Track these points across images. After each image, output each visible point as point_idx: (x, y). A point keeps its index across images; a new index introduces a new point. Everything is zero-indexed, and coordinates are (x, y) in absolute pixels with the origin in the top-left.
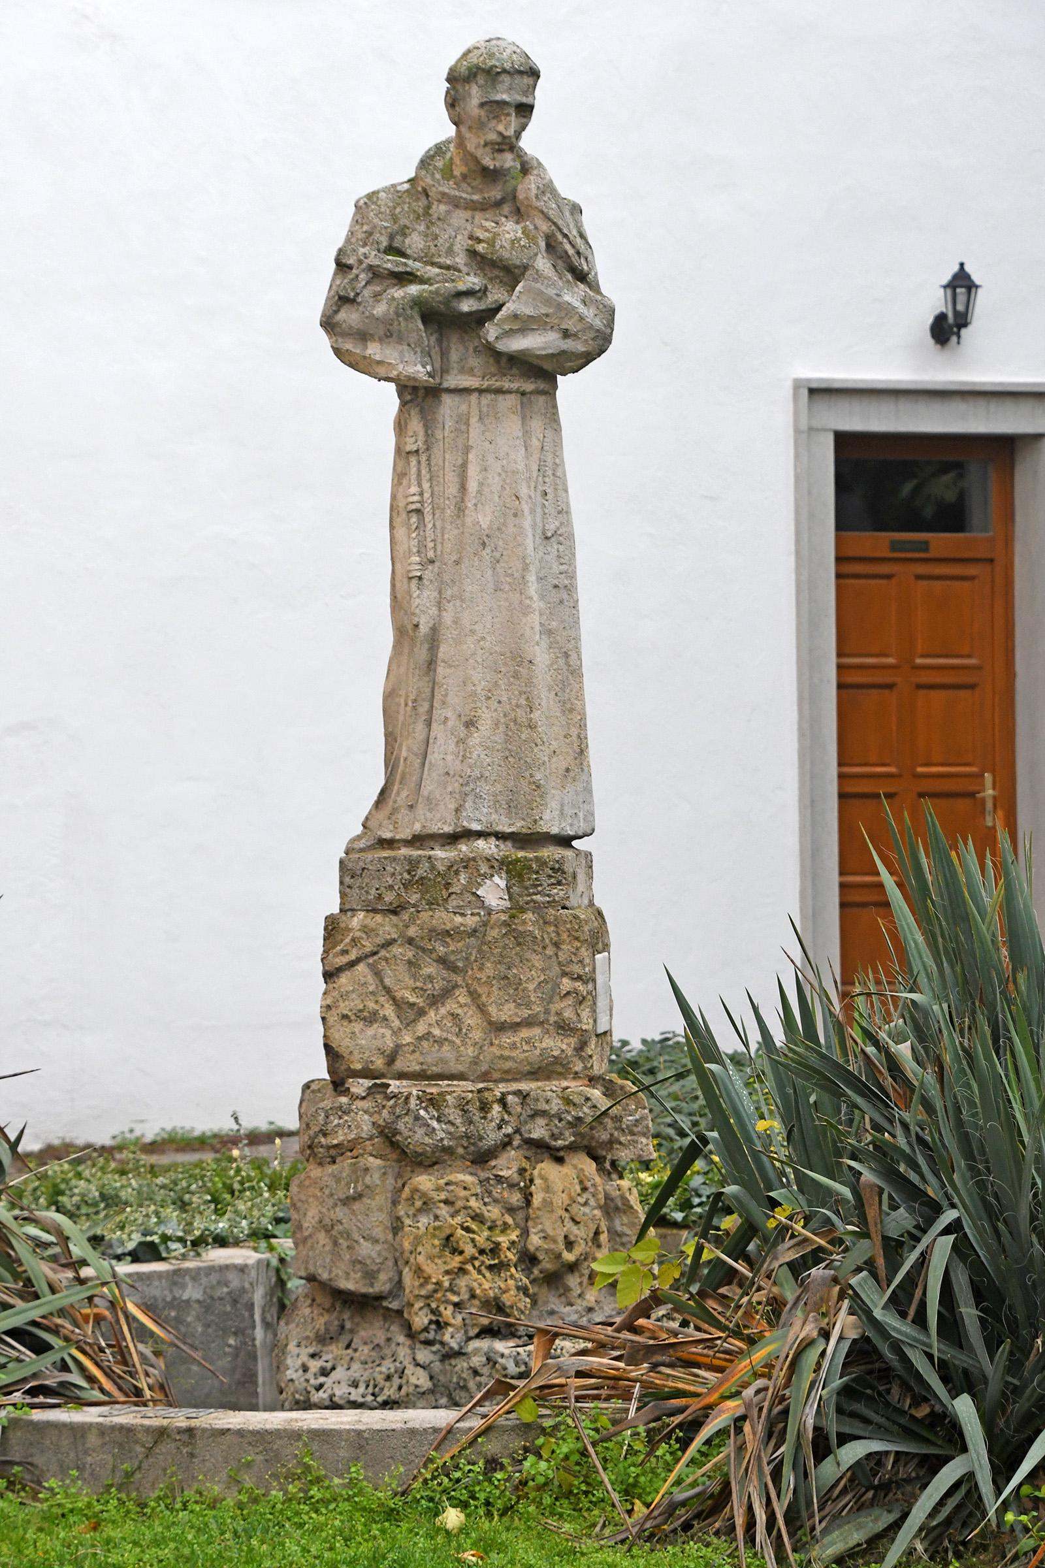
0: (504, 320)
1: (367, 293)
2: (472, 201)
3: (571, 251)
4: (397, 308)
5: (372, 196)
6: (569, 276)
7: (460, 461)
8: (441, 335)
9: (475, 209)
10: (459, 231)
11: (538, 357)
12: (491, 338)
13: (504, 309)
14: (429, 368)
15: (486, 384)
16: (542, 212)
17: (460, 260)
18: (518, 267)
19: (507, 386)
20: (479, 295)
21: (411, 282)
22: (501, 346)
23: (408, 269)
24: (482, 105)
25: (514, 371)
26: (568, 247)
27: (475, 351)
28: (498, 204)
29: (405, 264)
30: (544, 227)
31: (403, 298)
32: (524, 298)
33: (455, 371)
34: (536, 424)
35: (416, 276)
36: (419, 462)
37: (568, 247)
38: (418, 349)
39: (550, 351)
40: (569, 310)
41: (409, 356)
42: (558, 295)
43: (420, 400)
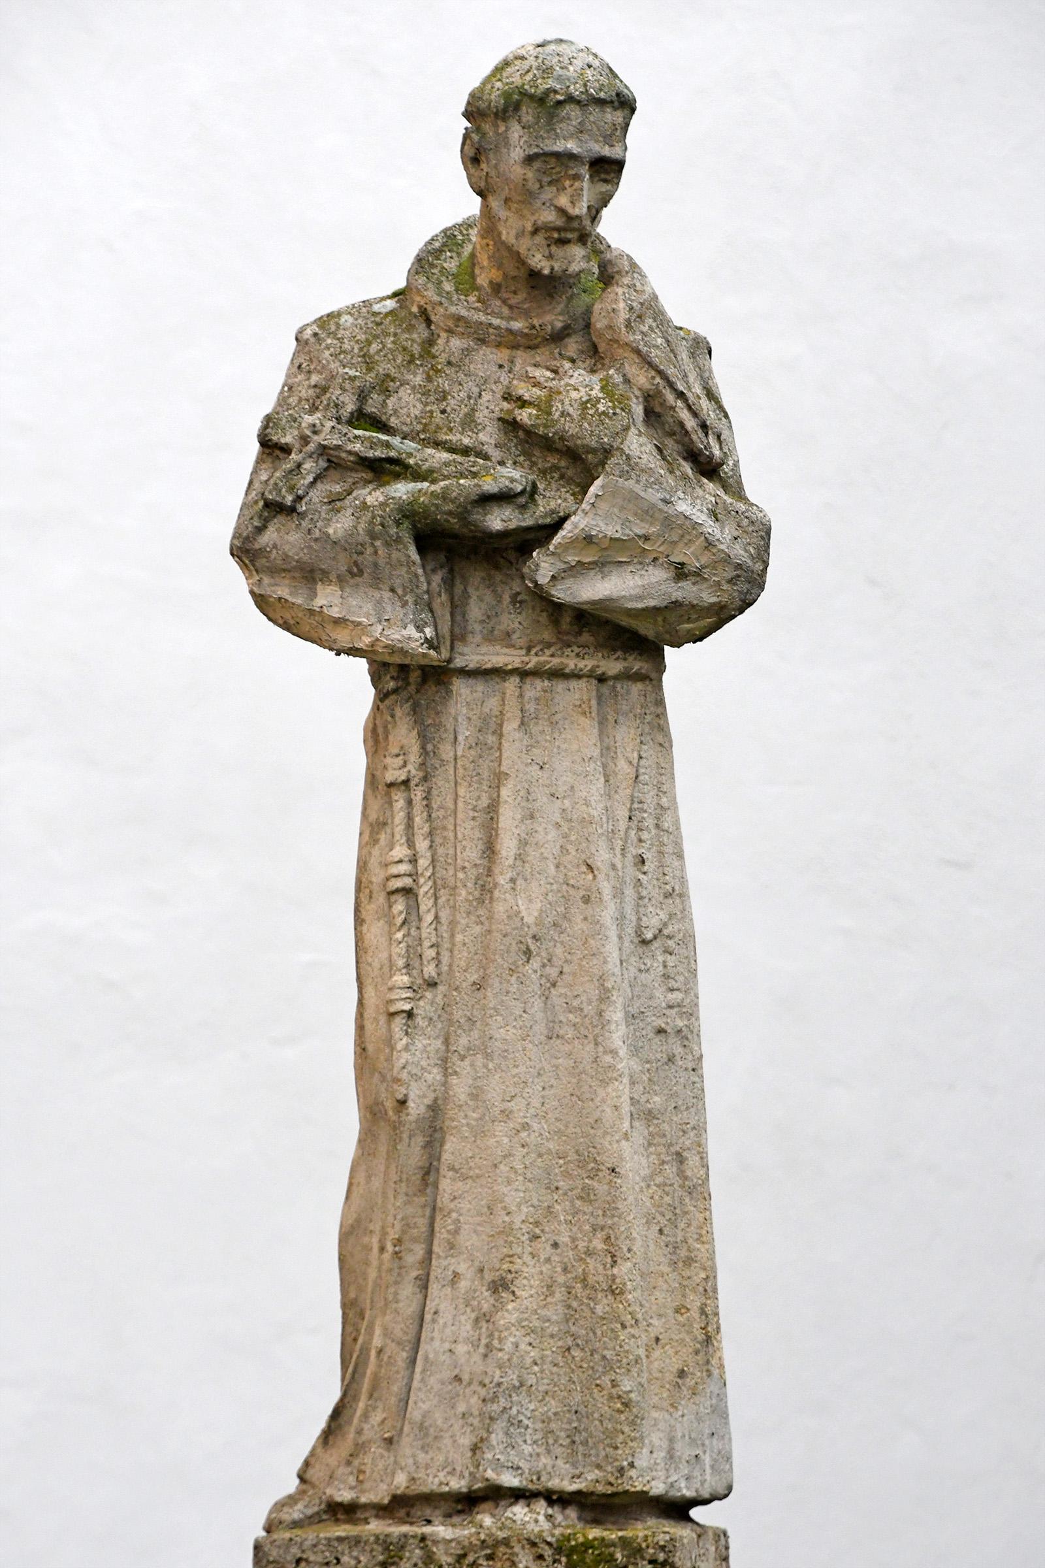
1: (316, 495)
2: (510, 331)
3: (690, 423)
4: (371, 523)
6: (687, 468)
7: (485, 801)
9: (515, 347)
10: (487, 383)
11: (630, 612)
12: (543, 578)
13: (568, 525)
14: (429, 632)
15: (533, 662)
16: (638, 352)
17: (488, 437)
18: (594, 451)
19: (571, 664)
20: (522, 500)
21: (397, 477)
22: (560, 593)
23: (393, 454)
24: (529, 160)
25: (586, 637)
26: (685, 415)
28: (558, 337)
29: (387, 445)
31: (383, 505)
32: (603, 506)
33: (478, 638)
34: (625, 735)
35: (407, 467)
36: (410, 802)
37: (685, 415)
38: (410, 599)
40: (689, 528)
41: (393, 610)
43: (412, 688)
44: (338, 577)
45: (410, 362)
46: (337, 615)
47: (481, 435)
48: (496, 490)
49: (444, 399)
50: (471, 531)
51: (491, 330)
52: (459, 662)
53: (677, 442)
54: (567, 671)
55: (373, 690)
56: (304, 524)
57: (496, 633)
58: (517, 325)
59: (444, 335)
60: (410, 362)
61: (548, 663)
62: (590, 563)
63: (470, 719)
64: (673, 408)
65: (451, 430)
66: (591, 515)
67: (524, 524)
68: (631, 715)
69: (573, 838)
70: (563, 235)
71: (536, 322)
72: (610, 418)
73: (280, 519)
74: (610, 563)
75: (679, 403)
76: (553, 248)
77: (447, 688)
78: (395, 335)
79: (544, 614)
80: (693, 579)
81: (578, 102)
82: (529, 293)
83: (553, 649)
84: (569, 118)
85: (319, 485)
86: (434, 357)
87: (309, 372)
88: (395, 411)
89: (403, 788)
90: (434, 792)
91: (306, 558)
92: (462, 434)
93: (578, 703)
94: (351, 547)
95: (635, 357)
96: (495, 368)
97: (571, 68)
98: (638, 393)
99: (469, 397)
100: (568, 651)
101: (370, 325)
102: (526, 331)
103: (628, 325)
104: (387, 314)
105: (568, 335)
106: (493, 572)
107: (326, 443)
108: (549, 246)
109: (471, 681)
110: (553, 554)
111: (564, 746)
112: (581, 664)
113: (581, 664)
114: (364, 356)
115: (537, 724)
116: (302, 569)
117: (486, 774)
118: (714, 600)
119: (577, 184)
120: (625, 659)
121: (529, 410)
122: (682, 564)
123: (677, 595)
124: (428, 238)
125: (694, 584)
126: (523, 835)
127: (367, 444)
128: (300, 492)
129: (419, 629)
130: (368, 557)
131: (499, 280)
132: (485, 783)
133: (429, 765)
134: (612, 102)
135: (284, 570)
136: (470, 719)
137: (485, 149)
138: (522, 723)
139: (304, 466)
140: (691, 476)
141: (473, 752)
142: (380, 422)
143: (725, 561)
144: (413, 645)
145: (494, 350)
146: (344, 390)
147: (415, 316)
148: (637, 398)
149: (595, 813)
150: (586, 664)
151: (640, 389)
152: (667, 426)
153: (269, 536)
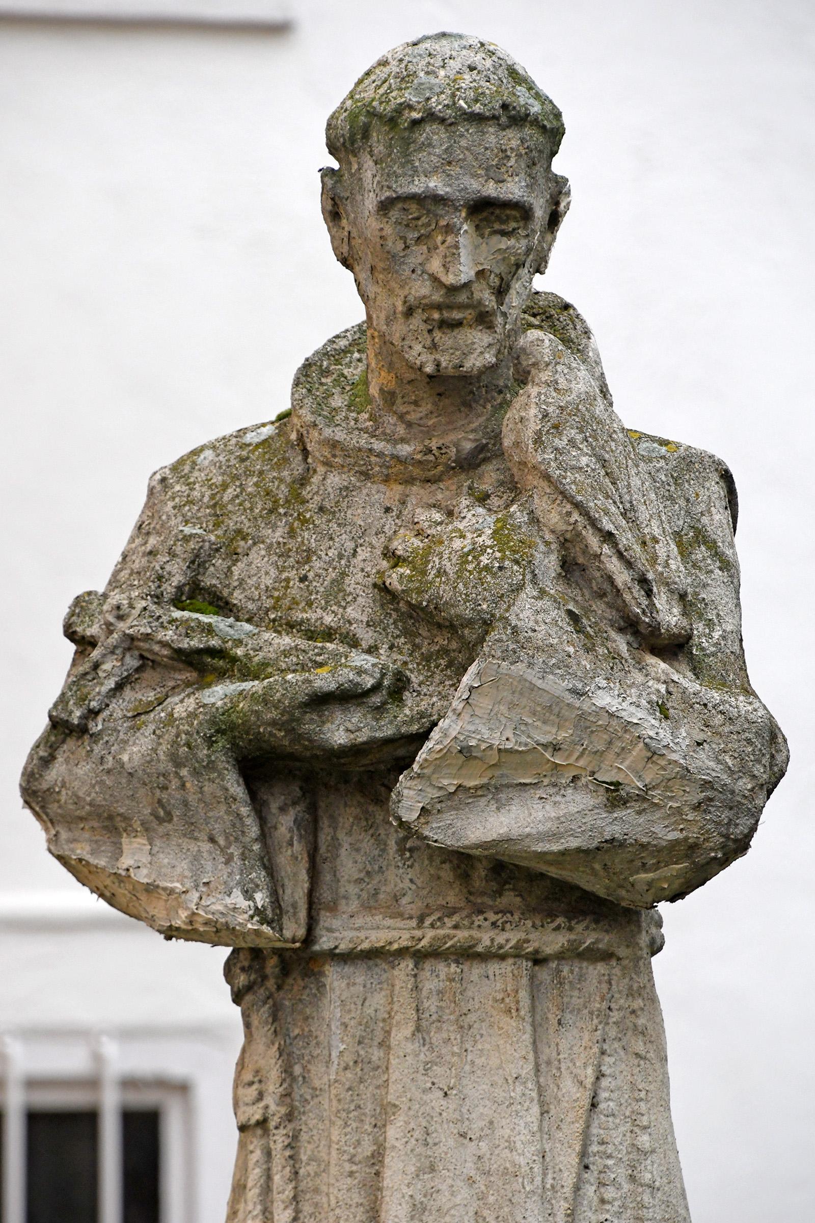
0: (442, 760)
1: (119, 708)
2: (396, 458)
3: (622, 577)
4: (174, 743)
5: (183, 467)
6: (621, 643)
7: (367, 1148)
8: (313, 809)
9: (409, 481)
10: (369, 533)
11: (541, 856)
12: (410, 815)
13: (435, 735)
14: (261, 898)
15: (427, 938)
16: (547, 477)
17: (359, 611)
18: (470, 623)
19: (486, 939)
20: (376, 699)
21: (222, 675)
22: (439, 832)
23: (214, 642)
24: (385, 207)
25: (509, 898)
26: (614, 565)
27: (401, 850)
28: (469, 464)
29: (209, 630)
30: (554, 516)
31: (192, 715)
32: (483, 703)
33: (354, 905)
34: (575, 1045)
35: (234, 660)
36: (268, 1154)
37: (614, 565)
38: (235, 850)
39: (574, 843)
40: (619, 731)
41: (214, 870)
42: (574, 692)
43: (271, 984)
44: (143, 824)
45: (271, 511)
46: (145, 881)
47: (349, 610)
48: (333, 686)
49: (308, 560)
50: (306, 748)
51: (373, 459)
52: (324, 943)
53: (610, 606)
54: (480, 949)
55: (228, 987)
56: (97, 748)
57: (381, 896)
58: (405, 450)
59: (321, 469)
60: (271, 511)
61: (450, 937)
62: (476, 788)
63: (346, 1026)
64: (597, 556)
65: (310, 604)
66: (466, 716)
67: (379, 735)
68: (586, 1011)
69: (491, 1199)
70: (446, 314)
71: (434, 445)
72: (494, 575)
73: (71, 744)
74: (508, 786)
75: (606, 549)
76: (437, 334)
77: (317, 979)
78: (261, 473)
79: (447, 866)
80: (637, 806)
81: (443, 121)
82: (435, 404)
83: (456, 918)
84: (430, 145)
85: (128, 693)
86: (304, 502)
87: (148, 533)
88: (241, 582)
89: (259, 1132)
90: (304, 1137)
91: (99, 800)
92: (324, 609)
93: (500, 996)
94: (152, 780)
95: (544, 484)
96: (379, 513)
97: (442, 73)
98: (549, 537)
99: (341, 556)
100: (478, 920)
101: (233, 462)
102: (418, 457)
103: (538, 440)
104: (258, 445)
105: (486, 460)
106: (371, 808)
107: (131, 631)
108: (430, 331)
109: (348, 969)
110: (419, 776)
111: (479, 1062)
112: (500, 939)
113: (500, 939)
114: (215, 506)
115: (439, 1029)
116: (99, 816)
117: (369, 1108)
118: (674, 835)
119: (450, 239)
120: (570, 929)
121: (402, 570)
122: (617, 784)
123: (614, 830)
124: (330, 336)
125: (639, 813)
126: (419, 1197)
127: (182, 630)
128: (94, 704)
129: (248, 895)
130: (173, 794)
131: (392, 386)
132: (368, 1120)
133: (296, 1096)
134: (495, 117)
135: (81, 819)
136: (346, 1026)
137: (341, 199)
138: (418, 1029)
139: (104, 667)
140: (626, 654)
141: (349, 1075)
142: (220, 598)
143: (683, 777)
144: (241, 918)
145: (382, 487)
146: (172, 554)
147: (293, 446)
148: (547, 544)
149: (522, 1161)
150: (509, 938)
151: (553, 532)
152: (594, 584)
153: (56, 772)
